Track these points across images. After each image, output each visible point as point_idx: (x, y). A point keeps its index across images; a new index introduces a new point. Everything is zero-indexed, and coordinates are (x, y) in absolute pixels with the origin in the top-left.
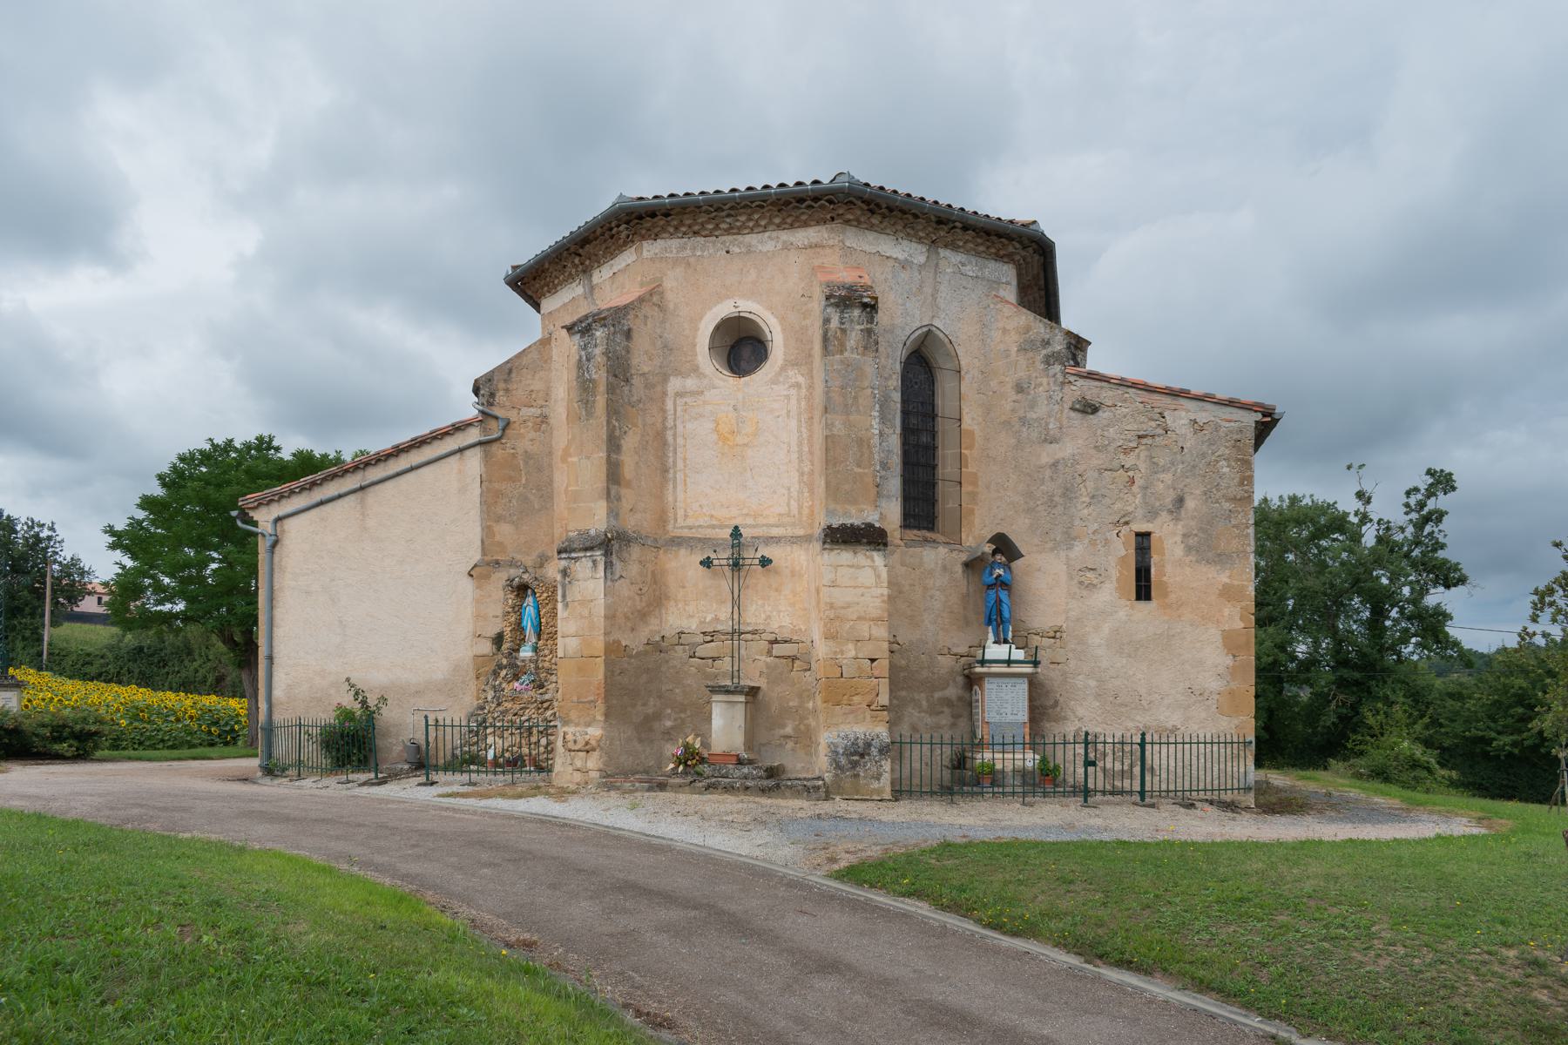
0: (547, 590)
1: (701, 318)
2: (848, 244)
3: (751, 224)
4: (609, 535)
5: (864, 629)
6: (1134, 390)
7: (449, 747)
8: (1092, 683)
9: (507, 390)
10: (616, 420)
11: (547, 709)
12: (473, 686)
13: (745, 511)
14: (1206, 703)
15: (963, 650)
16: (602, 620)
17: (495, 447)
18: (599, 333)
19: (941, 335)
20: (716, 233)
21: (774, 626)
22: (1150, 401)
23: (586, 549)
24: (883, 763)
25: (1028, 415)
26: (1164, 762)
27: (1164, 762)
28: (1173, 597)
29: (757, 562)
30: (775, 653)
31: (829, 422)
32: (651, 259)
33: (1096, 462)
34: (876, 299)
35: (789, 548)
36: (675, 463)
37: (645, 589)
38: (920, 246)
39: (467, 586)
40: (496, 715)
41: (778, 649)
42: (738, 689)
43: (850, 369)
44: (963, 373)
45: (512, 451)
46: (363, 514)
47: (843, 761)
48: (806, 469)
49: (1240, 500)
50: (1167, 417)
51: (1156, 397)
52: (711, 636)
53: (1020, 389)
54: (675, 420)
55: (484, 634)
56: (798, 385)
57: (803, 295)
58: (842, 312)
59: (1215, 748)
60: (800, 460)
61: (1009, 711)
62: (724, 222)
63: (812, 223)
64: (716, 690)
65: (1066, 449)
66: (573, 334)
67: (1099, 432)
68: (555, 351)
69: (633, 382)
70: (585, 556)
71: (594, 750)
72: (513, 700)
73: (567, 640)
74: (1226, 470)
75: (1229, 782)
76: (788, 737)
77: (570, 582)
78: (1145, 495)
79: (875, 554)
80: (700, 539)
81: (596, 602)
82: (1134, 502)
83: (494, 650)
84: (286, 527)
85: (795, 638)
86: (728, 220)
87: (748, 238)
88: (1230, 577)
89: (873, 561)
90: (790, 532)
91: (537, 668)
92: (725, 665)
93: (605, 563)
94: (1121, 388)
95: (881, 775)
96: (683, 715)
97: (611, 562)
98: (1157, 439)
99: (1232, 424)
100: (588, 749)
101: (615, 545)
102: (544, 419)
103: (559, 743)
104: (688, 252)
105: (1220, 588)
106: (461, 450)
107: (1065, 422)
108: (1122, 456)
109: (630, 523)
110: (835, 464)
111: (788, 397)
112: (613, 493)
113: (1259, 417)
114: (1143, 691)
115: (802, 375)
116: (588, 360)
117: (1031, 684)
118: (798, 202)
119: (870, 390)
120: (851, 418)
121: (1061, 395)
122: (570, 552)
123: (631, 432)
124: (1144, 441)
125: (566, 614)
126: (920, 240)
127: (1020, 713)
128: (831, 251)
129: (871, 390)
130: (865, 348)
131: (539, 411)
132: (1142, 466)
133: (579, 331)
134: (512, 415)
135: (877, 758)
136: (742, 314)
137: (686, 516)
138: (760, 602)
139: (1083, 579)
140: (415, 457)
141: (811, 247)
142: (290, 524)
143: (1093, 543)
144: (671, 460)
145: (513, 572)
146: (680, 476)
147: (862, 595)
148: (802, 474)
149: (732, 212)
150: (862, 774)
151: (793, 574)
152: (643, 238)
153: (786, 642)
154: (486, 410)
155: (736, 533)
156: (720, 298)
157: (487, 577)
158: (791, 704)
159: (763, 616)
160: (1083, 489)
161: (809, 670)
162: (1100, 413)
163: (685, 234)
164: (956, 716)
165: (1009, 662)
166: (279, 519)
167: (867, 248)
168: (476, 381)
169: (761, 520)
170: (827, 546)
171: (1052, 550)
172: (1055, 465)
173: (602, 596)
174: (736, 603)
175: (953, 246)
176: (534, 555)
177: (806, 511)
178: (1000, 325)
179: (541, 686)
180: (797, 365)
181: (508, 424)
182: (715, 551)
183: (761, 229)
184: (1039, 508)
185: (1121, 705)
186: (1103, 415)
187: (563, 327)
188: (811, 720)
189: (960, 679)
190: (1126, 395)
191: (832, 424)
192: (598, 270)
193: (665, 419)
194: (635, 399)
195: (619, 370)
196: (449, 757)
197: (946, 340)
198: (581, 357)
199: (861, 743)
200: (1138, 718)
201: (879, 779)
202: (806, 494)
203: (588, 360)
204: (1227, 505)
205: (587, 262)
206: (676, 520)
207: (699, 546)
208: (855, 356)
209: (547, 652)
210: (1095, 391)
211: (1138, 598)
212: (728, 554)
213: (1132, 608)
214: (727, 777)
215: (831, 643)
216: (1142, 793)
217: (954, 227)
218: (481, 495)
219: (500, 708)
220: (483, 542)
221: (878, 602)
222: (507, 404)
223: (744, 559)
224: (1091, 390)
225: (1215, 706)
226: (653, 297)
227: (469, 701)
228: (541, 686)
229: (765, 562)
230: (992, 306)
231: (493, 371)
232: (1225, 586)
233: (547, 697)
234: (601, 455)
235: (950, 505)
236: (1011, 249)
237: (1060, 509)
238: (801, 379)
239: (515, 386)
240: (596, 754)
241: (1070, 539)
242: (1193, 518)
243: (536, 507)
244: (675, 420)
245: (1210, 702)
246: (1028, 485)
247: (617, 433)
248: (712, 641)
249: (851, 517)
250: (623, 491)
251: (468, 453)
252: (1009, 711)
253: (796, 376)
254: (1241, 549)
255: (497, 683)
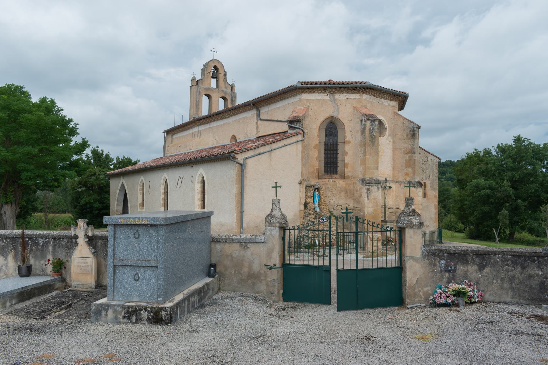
46: (270, 160)
51: (426, 153)
73: (369, 209)
84: (247, 162)
116: (373, 129)
125: (368, 202)
142: (249, 161)
155: (386, 180)
166: (246, 159)
251: (299, 143)
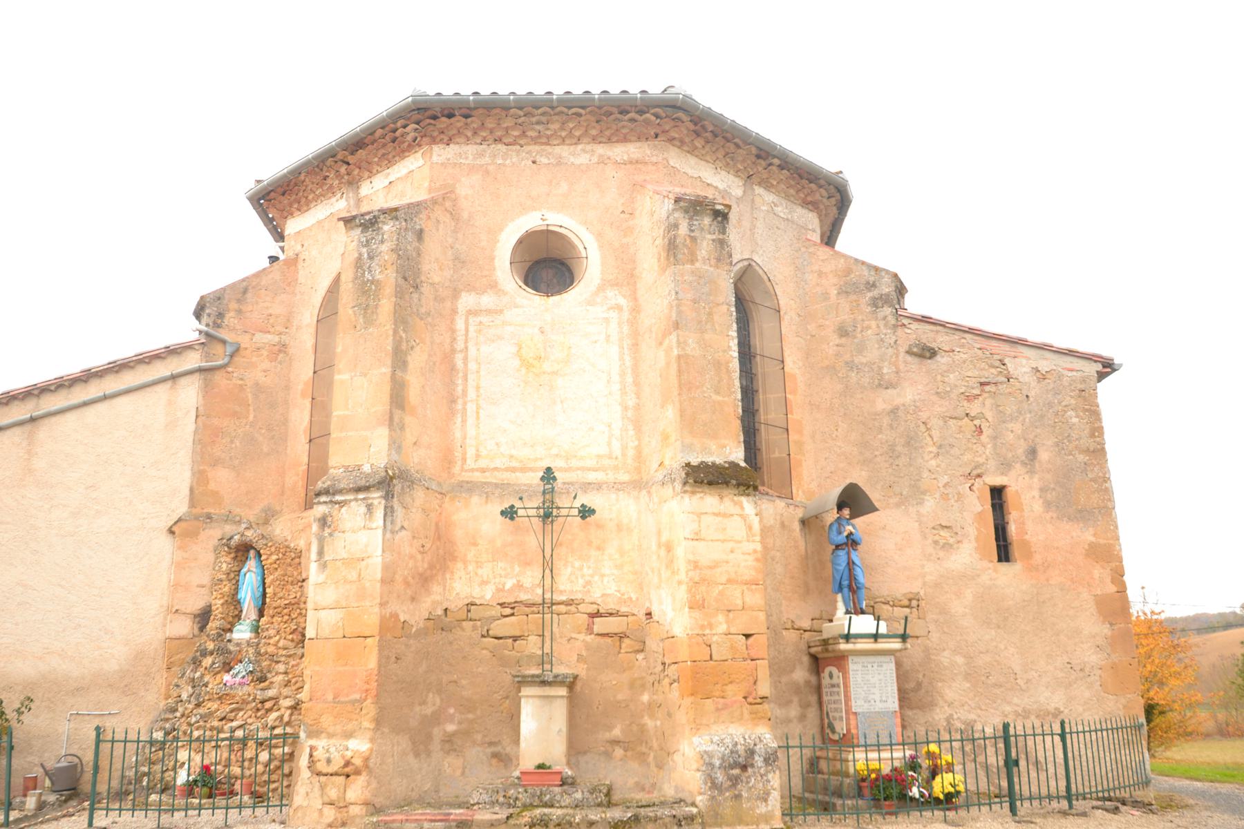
0: (278, 550)
1: (501, 230)
2: (672, 164)
3: (564, 134)
4: (390, 473)
5: (736, 595)
6: (970, 336)
7: (117, 765)
8: (960, 660)
9: (240, 312)
10: (404, 330)
11: (269, 710)
12: (161, 680)
13: (554, 451)
14: (1089, 680)
15: (806, 624)
16: (378, 585)
17: (218, 377)
18: (388, 227)
19: (761, 272)
20: (522, 142)
21: (596, 594)
22: (989, 348)
23: (359, 490)
24: (770, 776)
25: (856, 360)
26: (1050, 754)
27: (1050, 754)
28: (1038, 559)
29: (575, 512)
30: (596, 629)
31: (682, 340)
32: (442, 164)
33: (939, 409)
34: (729, 207)
35: (613, 496)
36: (465, 392)
37: (428, 546)
38: (736, 180)
39: (165, 545)
40: (194, 720)
41: (600, 625)
42: (559, 679)
43: (702, 281)
44: (782, 313)
45: (241, 382)
47: (720, 777)
48: (631, 404)
49: (1093, 452)
50: (1009, 365)
51: (994, 343)
52: (511, 608)
53: (843, 332)
54: (466, 342)
55: (183, 609)
56: (619, 308)
57: (623, 212)
58: (691, 219)
59: (1105, 733)
60: (623, 391)
61: (877, 697)
62: (533, 129)
63: (633, 138)
64: (524, 681)
65: (908, 394)
66: (352, 228)
67: (939, 377)
68: (301, 272)
69: (423, 290)
70: (356, 500)
71: (358, 772)
72: (220, 698)
73: (323, 614)
74: (1075, 420)
75: (1126, 780)
76: (616, 742)
77: (331, 535)
78: (995, 447)
79: (744, 499)
80: (496, 484)
81: (370, 561)
82: (985, 453)
83: (196, 631)
85: (624, 609)
86: (538, 127)
87: (558, 150)
88: (1094, 535)
89: (742, 508)
90: (611, 477)
91: (258, 654)
92: (532, 645)
93: (386, 507)
94: (957, 333)
95: (768, 794)
96: (470, 716)
97: (392, 507)
98: (1000, 387)
99: (1075, 373)
100: (348, 772)
101: (398, 486)
102: (282, 348)
103: (303, 761)
104: (487, 159)
105: (1086, 547)
106: (174, 378)
107: (902, 367)
108: (965, 404)
109: (419, 459)
110: (689, 389)
111: (607, 320)
112: (396, 419)
113: (1099, 367)
114: (1017, 668)
115: (624, 296)
116: (371, 258)
117: (899, 665)
118: (621, 113)
119: (725, 307)
120: (707, 336)
121: (894, 338)
122: (334, 494)
123: (417, 349)
124: (987, 388)
125: (322, 578)
126: (737, 173)
127: (890, 700)
128: (654, 168)
129: (727, 307)
130: (718, 260)
131: (277, 339)
132: (989, 415)
133: (361, 225)
134: (244, 341)
135: (762, 771)
136: (551, 228)
137: (478, 456)
138: (577, 564)
139: (937, 538)
140: (111, 384)
141: (631, 163)
143: (945, 497)
144: (460, 389)
145: (229, 529)
146: (471, 408)
147: (732, 552)
148: (626, 408)
149: (544, 119)
150: (745, 794)
151: (619, 527)
152: (434, 141)
153: (611, 614)
154: (212, 331)
155: (549, 475)
156: (524, 210)
157: (192, 534)
158: (620, 697)
159: (581, 581)
160: (928, 438)
161: (642, 651)
162: (938, 358)
163: (484, 139)
164: (805, 706)
165: (876, 637)
167: (690, 172)
168: (202, 298)
169: (574, 463)
170: (687, 488)
171: (898, 505)
172: (894, 411)
173: (379, 552)
174: (549, 566)
175: (768, 186)
176: (257, 509)
177: (631, 453)
178: (816, 268)
179: (262, 679)
180: (617, 285)
181: (237, 350)
182: (521, 499)
183: (574, 141)
184: (878, 459)
185: (995, 685)
186: (942, 360)
187: (340, 219)
188: (646, 718)
189: (806, 659)
190: (963, 341)
191: (685, 342)
192: (369, 181)
193: (454, 340)
194: (423, 310)
195: (410, 277)
196: (115, 784)
197: (765, 277)
198: (360, 255)
199: (740, 748)
200: (1016, 700)
201: (766, 800)
202: (631, 433)
203: (371, 258)
204: (1082, 458)
205: (356, 172)
206: (464, 460)
207: (497, 492)
208: (707, 267)
209: (272, 632)
210: (931, 335)
211: (1000, 560)
212: (537, 502)
213: (995, 571)
214: (552, 806)
215: (697, 614)
216: (1069, 797)
217: (770, 164)
218: (195, 432)
219: (201, 711)
220: (191, 490)
221: (751, 561)
222: (238, 327)
223: (558, 508)
224: (926, 335)
225: (1099, 683)
226: (444, 199)
227: (154, 698)
228: (262, 679)
229: (586, 512)
230: (803, 249)
231: (224, 289)
232: (1092, 545)
233: (271, 693)
234: (384, 370)
235: (777, 455)
236: (818, 197)
237: (902, 461)
238: (622, 301)
239: (250, 308)
240: (361, 780)
241: (918, 493)
242: (1049, 471)
243: (265, 450)
244: (466, 342)
245: (1092, 678)
246: (862, 434)
247: (404, 346)
248: (513, 615)
249: (711, 454)
250: (408, 419)
251: (183, 381)
252: (877, 697)
253: (615, 296)
254: (1102, 505)
255: (198, 675)
